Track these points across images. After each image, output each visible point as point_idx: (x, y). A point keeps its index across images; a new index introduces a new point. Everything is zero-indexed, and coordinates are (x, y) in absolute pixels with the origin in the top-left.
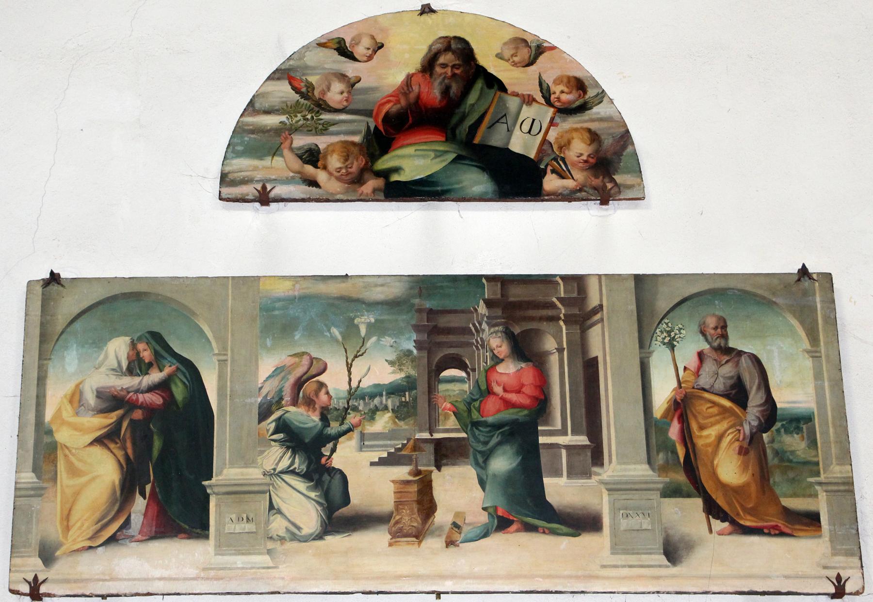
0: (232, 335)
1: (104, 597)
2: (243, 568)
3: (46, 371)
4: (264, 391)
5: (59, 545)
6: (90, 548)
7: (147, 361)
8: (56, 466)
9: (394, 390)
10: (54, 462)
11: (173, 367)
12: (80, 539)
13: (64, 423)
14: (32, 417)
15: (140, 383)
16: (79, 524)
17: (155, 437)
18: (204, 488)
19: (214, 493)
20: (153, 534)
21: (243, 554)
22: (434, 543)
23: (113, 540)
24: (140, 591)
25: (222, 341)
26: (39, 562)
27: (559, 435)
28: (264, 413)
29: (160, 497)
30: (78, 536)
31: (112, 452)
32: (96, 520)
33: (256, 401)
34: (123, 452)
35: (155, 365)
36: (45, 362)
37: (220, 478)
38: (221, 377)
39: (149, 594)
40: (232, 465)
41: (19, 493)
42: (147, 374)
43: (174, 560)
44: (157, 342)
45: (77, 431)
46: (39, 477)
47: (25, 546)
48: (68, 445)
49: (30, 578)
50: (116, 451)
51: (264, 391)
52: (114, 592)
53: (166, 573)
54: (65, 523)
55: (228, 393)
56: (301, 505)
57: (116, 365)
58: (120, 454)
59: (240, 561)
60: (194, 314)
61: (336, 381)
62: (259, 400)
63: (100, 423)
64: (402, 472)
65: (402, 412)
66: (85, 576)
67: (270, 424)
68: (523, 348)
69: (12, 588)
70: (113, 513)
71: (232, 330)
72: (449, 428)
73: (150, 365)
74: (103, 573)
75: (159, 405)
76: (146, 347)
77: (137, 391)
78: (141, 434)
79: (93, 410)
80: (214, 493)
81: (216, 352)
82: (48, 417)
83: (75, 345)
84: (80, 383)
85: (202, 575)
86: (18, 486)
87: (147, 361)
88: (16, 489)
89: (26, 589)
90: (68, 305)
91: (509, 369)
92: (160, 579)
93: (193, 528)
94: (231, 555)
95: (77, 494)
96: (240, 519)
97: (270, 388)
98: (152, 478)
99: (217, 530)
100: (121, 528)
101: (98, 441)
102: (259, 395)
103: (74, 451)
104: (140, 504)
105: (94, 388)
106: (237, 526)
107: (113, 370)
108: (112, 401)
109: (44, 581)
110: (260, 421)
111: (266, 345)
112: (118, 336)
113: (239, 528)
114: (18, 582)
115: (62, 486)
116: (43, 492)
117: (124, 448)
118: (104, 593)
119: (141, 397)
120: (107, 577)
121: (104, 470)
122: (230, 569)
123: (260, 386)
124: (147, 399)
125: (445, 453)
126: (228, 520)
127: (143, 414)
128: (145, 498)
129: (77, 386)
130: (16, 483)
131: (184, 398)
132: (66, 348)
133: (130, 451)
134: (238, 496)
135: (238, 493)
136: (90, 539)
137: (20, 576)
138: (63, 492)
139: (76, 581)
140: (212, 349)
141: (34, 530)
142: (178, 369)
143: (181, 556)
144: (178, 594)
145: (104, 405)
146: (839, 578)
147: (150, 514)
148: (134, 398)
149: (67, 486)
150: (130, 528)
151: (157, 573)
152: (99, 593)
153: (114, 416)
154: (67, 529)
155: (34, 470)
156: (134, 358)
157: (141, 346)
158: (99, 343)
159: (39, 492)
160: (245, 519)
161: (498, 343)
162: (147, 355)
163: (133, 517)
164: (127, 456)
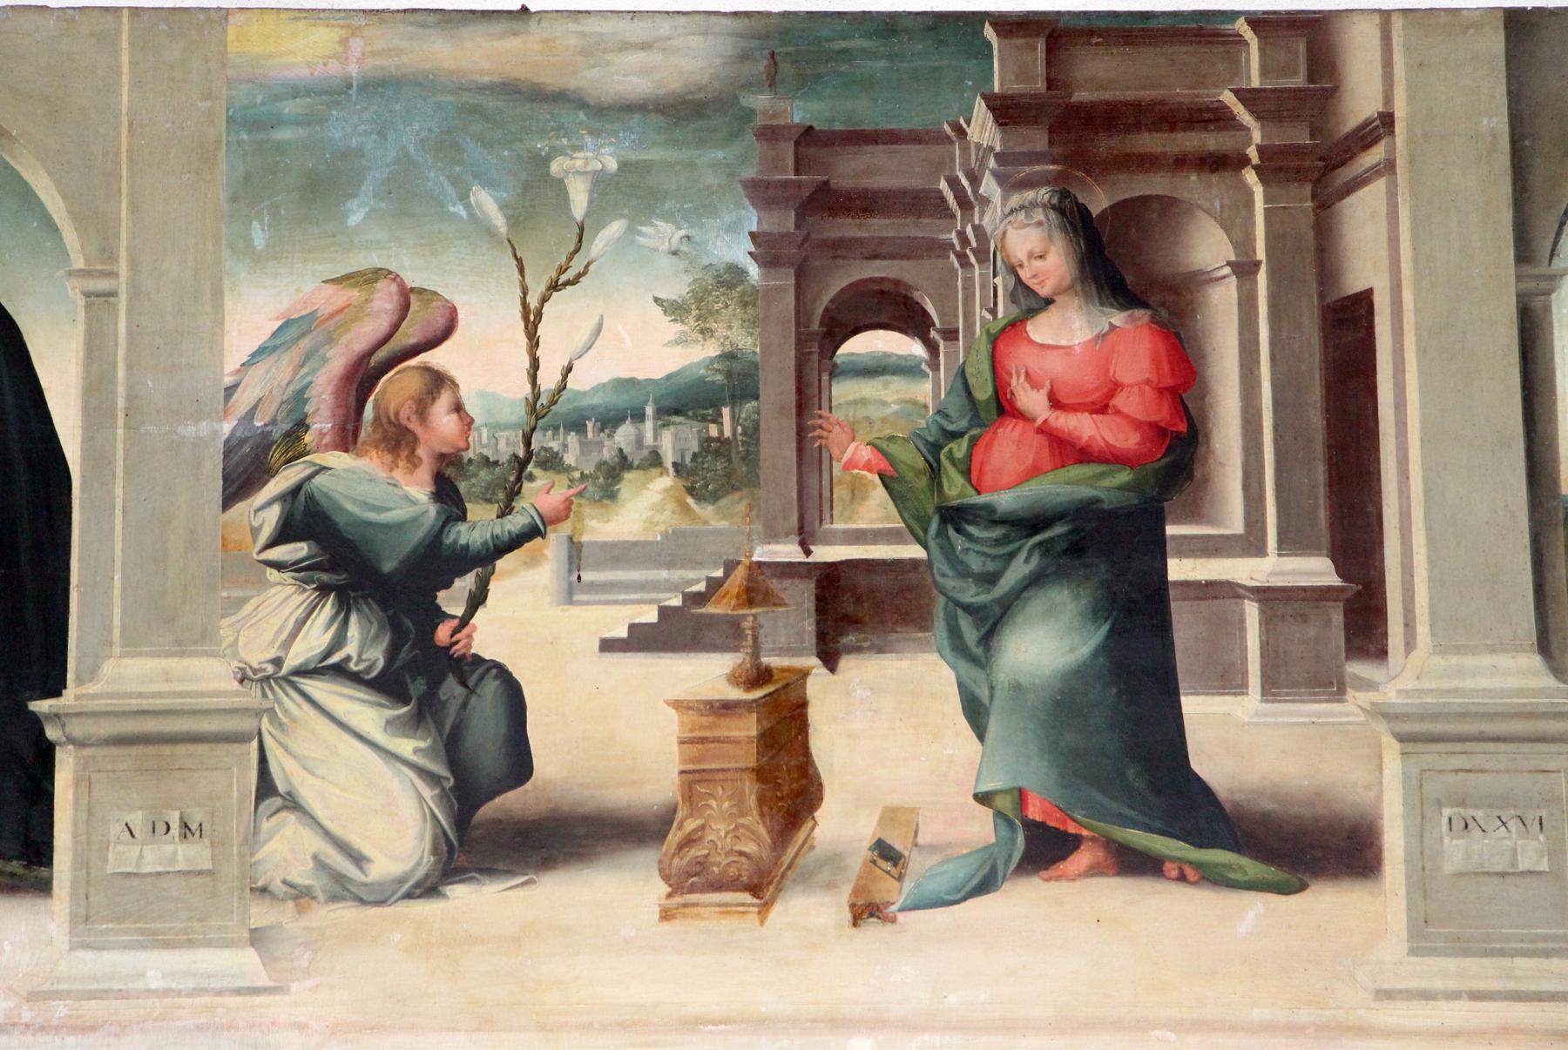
0: (134, 208)
2: (167, 992)
9: (684, 401)
18: (36, 723)
19: (70, 740)
21: (167, 945)
22: (809, 912)
27: (1236, 552)
28: (240, 480)
33: (215, 434)
37: (92, 688)
38: (96, 349)
40: (134, 644)
51: (243, 400)
55: (121, 403)
56: (365, 780)
59: (156, 967)
61: (486, 370)
62: (227, 428)
64: (709, 673)
65: (712, 474)
67: (262, 511)
68: (1117, 261)
72: (867, 528)
80: (70, 740)
81: (79, 263)
85: (27, 1015)
91: (1072, 331)
94: (126, 947)
97: (263, 391)
110: (228, 502)
111: (249, 241)
113: (155, 856)
122: (122, 995)
123: (228, 381)
125: (851, 608)
126: (116, 830)
134: (151, 749)
135: (152, 738)
161: (1034, 245)
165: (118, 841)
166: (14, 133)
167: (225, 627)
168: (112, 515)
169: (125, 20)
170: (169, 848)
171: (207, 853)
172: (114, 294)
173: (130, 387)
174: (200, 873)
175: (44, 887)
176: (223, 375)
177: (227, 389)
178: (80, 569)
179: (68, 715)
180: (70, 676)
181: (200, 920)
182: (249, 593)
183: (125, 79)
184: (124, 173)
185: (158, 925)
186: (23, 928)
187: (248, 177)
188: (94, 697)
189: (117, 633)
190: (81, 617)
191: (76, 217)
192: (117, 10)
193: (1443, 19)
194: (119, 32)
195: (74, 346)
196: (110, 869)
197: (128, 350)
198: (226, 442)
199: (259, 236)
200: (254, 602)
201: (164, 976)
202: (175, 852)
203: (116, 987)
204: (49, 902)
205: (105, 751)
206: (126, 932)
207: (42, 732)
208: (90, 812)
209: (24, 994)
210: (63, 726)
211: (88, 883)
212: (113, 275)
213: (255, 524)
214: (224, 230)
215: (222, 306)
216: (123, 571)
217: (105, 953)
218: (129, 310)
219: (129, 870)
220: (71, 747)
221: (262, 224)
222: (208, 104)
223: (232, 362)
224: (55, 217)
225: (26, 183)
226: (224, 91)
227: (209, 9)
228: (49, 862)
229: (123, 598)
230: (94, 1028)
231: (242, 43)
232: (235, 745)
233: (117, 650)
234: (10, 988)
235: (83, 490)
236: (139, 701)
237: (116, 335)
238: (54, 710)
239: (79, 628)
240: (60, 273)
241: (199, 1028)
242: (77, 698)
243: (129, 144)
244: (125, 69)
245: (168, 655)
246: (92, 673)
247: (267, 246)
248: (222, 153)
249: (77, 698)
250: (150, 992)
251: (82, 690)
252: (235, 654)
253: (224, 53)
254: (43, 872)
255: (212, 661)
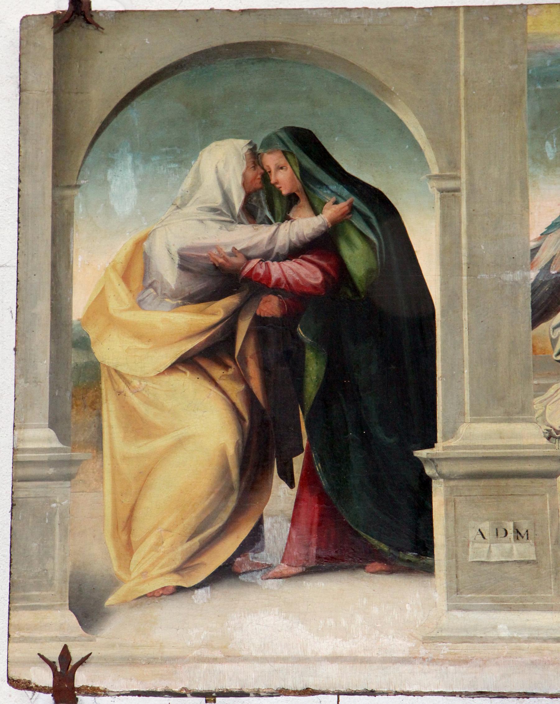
0: (470, 135)
1: (208, 696)
2: (511, 639)
3: (71, 214)
4: (543, 257)
5: (114, 583)
6: (179, 589)
7: (285, 192)
8: (100, 415)
10: (96, 406)
11: (343, 205)
12: (156, 572)
13: (112, 322)
14: (43, 308)
15: (273, 238)
16: (151, 540)
17: (309, 355)
18: (419, 464)
19: (441, 476)
20: (312, 563)
21: (510, 609)
23: (226, 573)
24: (290, 686)
25: (446, 146)
26: (71, 619)
29: (324, 483)
30: (153, 565)
31: (217, 385)
32: (189, 530)
33: (525, 279)
34: (242, 387)
35: (303, 201)
36: (68, 192)
37: (453, 442)
38: (448, 224)
39: (308, 692)
40: (479, 414)
41: (21, 472)
42: (286, 218)
43: (359, 619)
44: (308, 153)
45: (144, 340)
46: (62, 438)
47: (39, 586)
48: (123, 369)
49: (54, 655)
50: (226, 384)
51: (543, 257)
52: (234, 687)
53: (344, 648)
54: (124, 537)
55: (465, 260)
57: (219, 201)
58: (235, 390)
59: (504, 622)
60: (384, 89)
62: (533, 275)
63: (195, 322)
66: (169, 652)
69: (15, 675)
70: (224, 516)
71: (468, 122)
73: (292, 200)
74: (209, 646)
75: (314, 287)
76: (282, 161)
77: (266, 257)
78: (278, 344)
79: (174, 296)
80: (441, 476)
81: (435, 171)
82: (79, 305)
83: (130, 158)
84: (145, 238)
85: (423, 652)
86: (20, 456)
87: (285, 192)
88: (15, 463)
89: (45, 677)
90: (112, 70)
92: (333, 659)
93: (399, 550)
94: (483, 609)
95: (145, 476)
96: (500, 533)
98: (305, 442)
99: (453, 555)
100: (242, 550)
101: (187, 362)
102: (532, 266)
103: (136, 383)
104: (281, 497)
105: (174, 250)
106: (494, 547)
107: (214, 210)
108: (216, 278)
109: (83, 661)
110: (535, 322)
111: (543, 154)
112: (221, 138)
113: (498, 551)
114: (28, 663)
115: (113, 457)
116: (73, 470)
117: (243, 378)
118: (212, 687)
119: (276, 270)
120: (217, 654)
121: (204, 425)
122: (483, 640)
123: (533, 245)
124: (289, 273)
126: (473, 534)
127: (281, 305)
128: (291, 485)
129: (139, 244)
130: (15, 451)
131: (370, 272)
132: (110, 162)
133: (256, 385)
134: (493, 482)
135: (495, 475)
136: (178, 571)
137: (31, 651)
138: (116, 471)
139: (150, 662)
140: (425, 165)
141: (58, 553)
142: (352, 208)
143: (375, 610)
144: (372, 693)
145: (197, 286)
146: (65, 654)
147: (303, 519)
148: (261, 271)
149: (125, 458)
150: (262, 549)
151: (326, 646)
152: (201, 688)
153: (219, 310)
154: (129, 548)
155: (53, 425)
156: (258, 184)
157: (272, 160)
158: (181, 149)
159: (65, 470)
160: (511, 531)
162: (285, 179)
163: (267, 525)
164: (249, 394)
165: (475, 541)
166: (393, 89)
167: (537, 404)
168: (461, 332)
169: (462, 14)
170: (507, 546)
171: (533, 549)
172: (458, 190)
173: (470, 249)
174: (528, 562)
175: (429, 570)
176: (529, 241)
177: (532, 250)
178: (442, 366)
179: (438, 459)
180: (439, 435)
181: (530, 593)
182: (551, 381)
183: (462, 52)
184: (463, 112)
185: (503, 596)
186: (417, 595)
187: (542, 113)
188: (455, 448)
189: (467, 408)
190: (445, 396)
191: (432, 141)
192: (456, 8)
193: (24, 43)
194: (457, 22)
195: (434, 224)
196: (471, 558)
197: (468, 226)
198: (533, 284)
199: (550, 151)
200: (555, 387)
201: (509, 628)
202: (512, 548)
203: (479, 635)
204: (433, 579)
205: (464, 483)
206: (483, 600)
207: (423, 470)
208: (456, 522)
209: (421, 638)
210: (436, 466)
211: (457, 568)
212: (459, 178)
213: (553, 337)
214: (528, 147)
215: (527, 196)
216: (470, 367)
217: (470, 613)
218: (468, 201)
219: (483, 559)
220: (442, 480)
221: (552, 144)
222: (515, 67)
223: (536, 231)
224: (420, 142)
225: (400, 121)
226: (526, 58)
227: (515, 6)
228: (432, 555)
229: (471, 385)
230: (466, 662)
231: (538, 27)
232: (546, 480)
233: (468, 418)
234: (411, 635)
235: (443, 315)
236: (484, 451)
237: (460, 216)
238: (430, 456)
239: (444, 403)
240: (424, 177)
241: (533, 663)
242: (444, 448)
243: (466, 93)
244: (462, 46)
245: (500, 421)
246: (452, 433)
247: (556, 157)
248: (525, 98)
249: (444, 448)
250: (501, 639)
251: (447, 444)
252: (544, 421)
253: (525, 34)
254: (428, 560)
255: (529, 425)
